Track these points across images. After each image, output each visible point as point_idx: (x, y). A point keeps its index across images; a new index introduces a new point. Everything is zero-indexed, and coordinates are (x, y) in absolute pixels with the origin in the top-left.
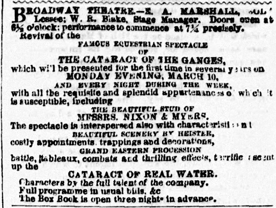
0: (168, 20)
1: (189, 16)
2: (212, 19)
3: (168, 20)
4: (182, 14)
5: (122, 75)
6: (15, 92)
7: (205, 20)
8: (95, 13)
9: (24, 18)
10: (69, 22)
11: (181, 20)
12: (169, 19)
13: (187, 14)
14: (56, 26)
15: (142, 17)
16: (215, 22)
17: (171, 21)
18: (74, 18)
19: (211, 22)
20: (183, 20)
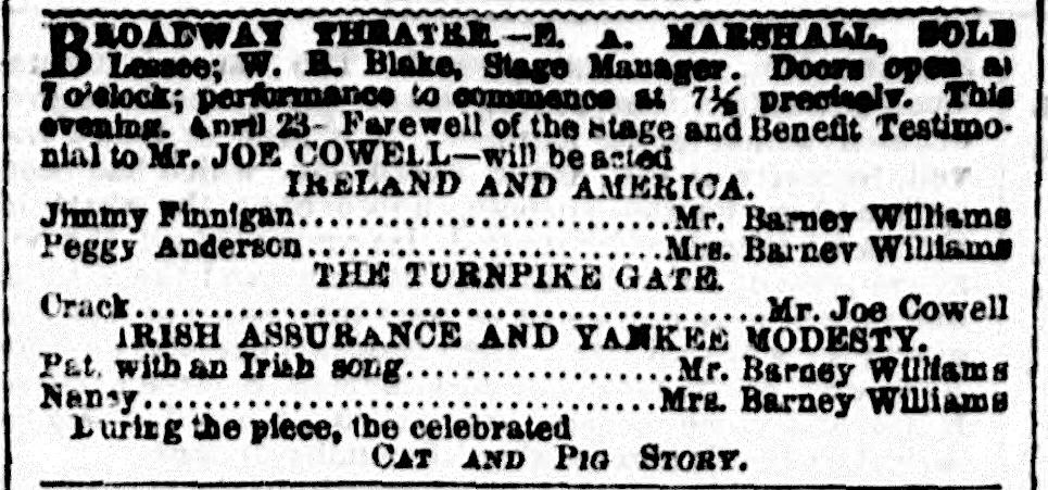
0: (615, 69)
1: (696, 56)
2: (777, 68)
3: (615, 69)
4: (670, 46)
5: (262, 337)
6: (955, 305)
7: (752, 70)
8: (344, 42)
9: (85, 64)
10: (236, 78)
11: (661, 69)
12: (619, 63)
13: (688, 46)
14: (168, 91)
15: (514, 57)
16: (787, 77)
17: (626, 72)
18: (256, 64)
19: (776, 76)
20: (531, 66)
